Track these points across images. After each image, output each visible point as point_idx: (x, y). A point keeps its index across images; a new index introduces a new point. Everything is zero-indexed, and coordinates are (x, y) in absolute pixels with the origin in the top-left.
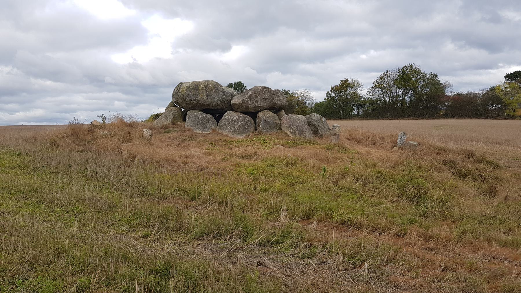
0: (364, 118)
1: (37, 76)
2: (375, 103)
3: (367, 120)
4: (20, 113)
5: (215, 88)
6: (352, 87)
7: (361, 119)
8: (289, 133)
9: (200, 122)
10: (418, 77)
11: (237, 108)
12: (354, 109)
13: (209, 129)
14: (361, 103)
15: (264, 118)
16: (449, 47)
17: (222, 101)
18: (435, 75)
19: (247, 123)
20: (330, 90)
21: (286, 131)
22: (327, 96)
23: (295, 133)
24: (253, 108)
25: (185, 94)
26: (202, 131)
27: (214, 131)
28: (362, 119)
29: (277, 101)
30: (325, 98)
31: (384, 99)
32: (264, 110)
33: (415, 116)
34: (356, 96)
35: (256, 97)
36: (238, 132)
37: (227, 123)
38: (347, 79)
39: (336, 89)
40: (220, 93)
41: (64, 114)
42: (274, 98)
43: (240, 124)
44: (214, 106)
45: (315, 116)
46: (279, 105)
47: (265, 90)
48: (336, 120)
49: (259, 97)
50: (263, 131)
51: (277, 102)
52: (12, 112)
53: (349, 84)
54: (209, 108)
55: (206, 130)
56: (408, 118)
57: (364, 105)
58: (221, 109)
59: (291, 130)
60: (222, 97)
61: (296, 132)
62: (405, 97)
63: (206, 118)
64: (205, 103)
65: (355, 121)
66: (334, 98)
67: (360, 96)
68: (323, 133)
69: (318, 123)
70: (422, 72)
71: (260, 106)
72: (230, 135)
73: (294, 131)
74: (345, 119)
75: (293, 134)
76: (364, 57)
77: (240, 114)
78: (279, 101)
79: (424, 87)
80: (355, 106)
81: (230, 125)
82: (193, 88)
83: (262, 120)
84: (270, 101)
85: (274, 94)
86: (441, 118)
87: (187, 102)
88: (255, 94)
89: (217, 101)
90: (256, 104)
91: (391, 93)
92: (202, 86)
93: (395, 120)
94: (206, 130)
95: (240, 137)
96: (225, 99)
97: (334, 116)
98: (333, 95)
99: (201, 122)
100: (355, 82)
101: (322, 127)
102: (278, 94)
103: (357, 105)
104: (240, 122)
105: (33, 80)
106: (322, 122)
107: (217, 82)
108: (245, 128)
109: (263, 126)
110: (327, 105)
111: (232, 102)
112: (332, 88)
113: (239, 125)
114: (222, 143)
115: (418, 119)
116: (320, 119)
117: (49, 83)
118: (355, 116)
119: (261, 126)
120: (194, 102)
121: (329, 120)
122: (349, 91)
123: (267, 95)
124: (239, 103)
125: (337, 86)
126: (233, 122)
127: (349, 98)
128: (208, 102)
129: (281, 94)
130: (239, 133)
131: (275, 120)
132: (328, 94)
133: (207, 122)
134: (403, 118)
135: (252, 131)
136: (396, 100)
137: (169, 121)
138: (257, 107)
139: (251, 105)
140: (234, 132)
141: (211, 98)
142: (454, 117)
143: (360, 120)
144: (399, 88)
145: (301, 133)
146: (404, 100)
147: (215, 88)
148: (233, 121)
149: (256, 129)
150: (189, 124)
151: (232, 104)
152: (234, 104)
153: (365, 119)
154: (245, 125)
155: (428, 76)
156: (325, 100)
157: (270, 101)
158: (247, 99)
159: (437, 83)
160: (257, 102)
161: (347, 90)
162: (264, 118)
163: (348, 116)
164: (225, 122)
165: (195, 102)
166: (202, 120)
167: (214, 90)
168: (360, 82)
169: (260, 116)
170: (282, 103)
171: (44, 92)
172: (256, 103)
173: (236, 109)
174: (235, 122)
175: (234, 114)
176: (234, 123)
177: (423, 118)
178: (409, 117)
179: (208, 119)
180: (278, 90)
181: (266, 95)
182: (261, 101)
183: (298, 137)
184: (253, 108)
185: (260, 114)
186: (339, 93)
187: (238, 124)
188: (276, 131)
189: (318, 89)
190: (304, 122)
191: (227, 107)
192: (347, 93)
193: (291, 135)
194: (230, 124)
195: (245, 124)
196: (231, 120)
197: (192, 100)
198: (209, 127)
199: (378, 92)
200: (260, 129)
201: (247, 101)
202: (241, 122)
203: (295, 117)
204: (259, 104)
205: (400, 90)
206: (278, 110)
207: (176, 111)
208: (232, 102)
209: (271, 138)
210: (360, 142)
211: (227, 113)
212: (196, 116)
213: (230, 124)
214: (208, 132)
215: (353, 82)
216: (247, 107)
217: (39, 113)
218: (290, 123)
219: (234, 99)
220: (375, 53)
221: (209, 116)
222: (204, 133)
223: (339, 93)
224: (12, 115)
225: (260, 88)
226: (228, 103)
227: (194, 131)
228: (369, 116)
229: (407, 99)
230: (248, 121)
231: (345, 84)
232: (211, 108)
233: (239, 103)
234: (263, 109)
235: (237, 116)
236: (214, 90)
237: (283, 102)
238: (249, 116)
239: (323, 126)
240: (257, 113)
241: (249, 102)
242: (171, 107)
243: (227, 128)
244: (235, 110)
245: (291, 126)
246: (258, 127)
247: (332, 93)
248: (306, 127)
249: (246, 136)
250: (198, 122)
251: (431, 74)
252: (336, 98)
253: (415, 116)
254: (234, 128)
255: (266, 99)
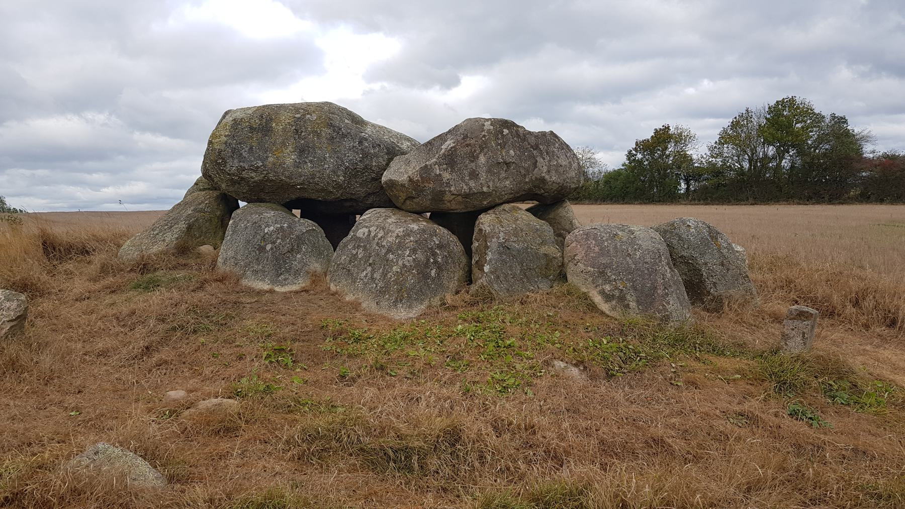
0: (699, 200)
1: (144, 129)
2: (720, 173)
3: (706, 204)
4: (110, 188)
5: (331, 125)
6: (676, 143)
7: (693, 202)
8: (598, 299)
9: (269, 247)
10: (808, 122)
11: (403, 196)
12: (680, 184)
13: (297, 273)
14: (694, 174)
15: (502, 235)
16: (844, 74)
17: (353, 173)
18: (842, 118)
19: (434, 255)
20: (634, 147)
21: (584, 290)
22: (629, 159)
23: (622, 299)
24: (460, 198)
25: (223, 147)
26: (273, 282)
27: (316, 279)
28: (696, 202)
29: (549, 172)
30: (625, 163)
31: (740, 165)
32: (502, 204)
33: (802, 199)
34: (688, 159)
35: (474, 158)
36: (399, 291)
37: (360, 256)
38: (667, 126)
39: (644, 146)
40: (348, 143)
41: (178, 190)
42: (539, 159)
43: (408, 260)
44: (323, 190)
45: (689, 226)
46: (555, 187)
47: (506, 131)
48: (645, 204)
49: (482, 159)
50: (496, 286)
51: (547, 177)
52: (97, 186)
53: (670, 137)
54: (306, 195)
55: (285, 280)
56: (787, 201)
57: (700, 176)
58: (351, 199)
59: (607, 288)
60: (350, 157)
61: (628, 297)
62: (781, 161)
63: (292, 233)
64: (290, 178)
65: (683, 206)
66: (640, 162)
67: (691, 160)
68: (721, 290)
69: (702, 254)
70: (817, 111)
71: (485, 189)
72: (369, 305)
73: (617, 293)
74: (662, 201)
75: (614, 303)
76: (691, 91)
77: (414, 221)
78: (556, 171)
79: (820, 140)
80: (682, 178)
81: (370, 265)
82: (251, 128)
83: (493, 244)
84: (523, 172)
85: (536, 147)
86: (856, 203)
87: (229, 174)
88: (468, 145)
89: (334, 171)
90: (472, 184)
91: (753, 154)
92: (285, 118)
93: (762, 206)
94: (285, 280)
95: (401, 314)
96: (361, 166)
97: (642, 197)
98: (639, 156)
99: (272, 249)
100: (681, 133)
101: (718, 268)
102: (551, 149)
103: (684, 176)
104: (408, 252)
105: (137, 135)
106: (719, 250)
107: (345, 109)
108: (426, 276)
109: (496, 270)
110: (628, 177)
111: (386, 177)
112: (637, 144)
113: (404, 266)
114: (328, 345)
115: (808, 203)
116: (712, 237)
117: (162, 141)
118: (680, 196)
119: (486, 268)
120: (253, 175)
121: (632, 203)
122: (670, 150)
123: (512, 152)
124: (411, 180)
125: (648, 141)
126: (384, 251)
127: (671, 162)
128: (301, 176)
129: (563, 149)
130: (403, 296)
131: (543, 243)
132: (630, 155)
133: (292, 250)
134: (778, 201)
135: (453, 285)
136: (762, 166)
137: (167, 240)
138: (474, 194)
139: (452, 189)
140: (382, 292)
141: (311, 161)
142: (881, 201)
143: (692, 205)
144: (770, 144)
145: (647, 299)
146: (779, 165)
147: (331, 125)
148: (383, 246)
149: (469, 279)
150: (230, 253)
151: (386, 183)
152: (392, 184)
153: (702, 202)
154: (427, 265)
155: (827, 121)
156: (623, 166)
157: (523, 172)
158: (440, 165)
159: (847, 134)
160: (474, 175)
161: (666, 148)
162: (502, 235)
163: (670, 197)
164: (354, 252)
165: (256, 177)
166: (274, 243)
167: (326, 132)
168: (692, 132)
169: (486, 228)
170: (564, 180)
171: (154, 154)
172: (471, 179)
173: (401, 200)
174: (389, 251)
175: (389, 221)
176: (387, 253)
177: (818, 203)
178: (790, 199)
179: (297, 237)
180: (552, 132)
181: (508, 152)
182: (489, 171)
183: (635, 314)
184: (460, 198)
185: (486, 221)
186: (652, 153)
187: (400, 263)
188: (544, 286)
189: (608, 148)
190: (660, 256)
191: (374, 193)
192: (667, 153)
193: (605, 307)
194: (371, 261)
195: (428, 260)
196: (378, 244)
197: (244, 169)
198: (299, 266)
199: (728, 150)
200: (483, 281)
201: (438, 172)
202: (414, 251)
203: (620, 233)
204: (485, 183)
205: (771, 148)
206: (549, 202)
207: (201, 207)
208: (386, 177)
209: (528, 323)
210: (830, 313)
211: (368, 215)
212: (257, 226)
213: (371, 261)
214: (295, 288)
215: (679, 132)
216: (438, 196)
217: (138, 188)
218: (604, 260)
219: (396, 164)
220: (711, 83)
221: (308, 225)
222: (277, 289)
223: (652, 153)
224: (97, 191)
225: (489, 123)
226: (373, 179)
227: (245, 282)
228: (711, 197)
229: (786, 163)
230: (440, 246)
231: (663, 137)
232: (314, 196)
233: (411, 180)
234: (497, 201)
235: (400, 231)
236: (326, 132)
237: (569, 176)
238: (446, 231)
239: (723, 265)
240: (476, 218)
241: (446, 176)
242: (200, 190)
243: (358, 273)
244: (399, 205)
245: (608, 271)
246: (475, 270)
247: (638, 153)
248: (669, 275)
249: (429, 307)
250: (262, 249)
251: (833, 116)
252: (646, 163)
253: (802, 199)
254: (384, 275)
255: (508, 164)
